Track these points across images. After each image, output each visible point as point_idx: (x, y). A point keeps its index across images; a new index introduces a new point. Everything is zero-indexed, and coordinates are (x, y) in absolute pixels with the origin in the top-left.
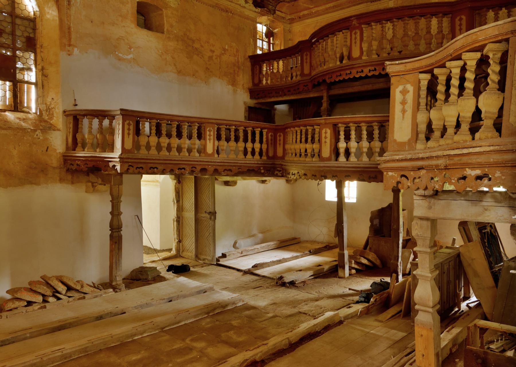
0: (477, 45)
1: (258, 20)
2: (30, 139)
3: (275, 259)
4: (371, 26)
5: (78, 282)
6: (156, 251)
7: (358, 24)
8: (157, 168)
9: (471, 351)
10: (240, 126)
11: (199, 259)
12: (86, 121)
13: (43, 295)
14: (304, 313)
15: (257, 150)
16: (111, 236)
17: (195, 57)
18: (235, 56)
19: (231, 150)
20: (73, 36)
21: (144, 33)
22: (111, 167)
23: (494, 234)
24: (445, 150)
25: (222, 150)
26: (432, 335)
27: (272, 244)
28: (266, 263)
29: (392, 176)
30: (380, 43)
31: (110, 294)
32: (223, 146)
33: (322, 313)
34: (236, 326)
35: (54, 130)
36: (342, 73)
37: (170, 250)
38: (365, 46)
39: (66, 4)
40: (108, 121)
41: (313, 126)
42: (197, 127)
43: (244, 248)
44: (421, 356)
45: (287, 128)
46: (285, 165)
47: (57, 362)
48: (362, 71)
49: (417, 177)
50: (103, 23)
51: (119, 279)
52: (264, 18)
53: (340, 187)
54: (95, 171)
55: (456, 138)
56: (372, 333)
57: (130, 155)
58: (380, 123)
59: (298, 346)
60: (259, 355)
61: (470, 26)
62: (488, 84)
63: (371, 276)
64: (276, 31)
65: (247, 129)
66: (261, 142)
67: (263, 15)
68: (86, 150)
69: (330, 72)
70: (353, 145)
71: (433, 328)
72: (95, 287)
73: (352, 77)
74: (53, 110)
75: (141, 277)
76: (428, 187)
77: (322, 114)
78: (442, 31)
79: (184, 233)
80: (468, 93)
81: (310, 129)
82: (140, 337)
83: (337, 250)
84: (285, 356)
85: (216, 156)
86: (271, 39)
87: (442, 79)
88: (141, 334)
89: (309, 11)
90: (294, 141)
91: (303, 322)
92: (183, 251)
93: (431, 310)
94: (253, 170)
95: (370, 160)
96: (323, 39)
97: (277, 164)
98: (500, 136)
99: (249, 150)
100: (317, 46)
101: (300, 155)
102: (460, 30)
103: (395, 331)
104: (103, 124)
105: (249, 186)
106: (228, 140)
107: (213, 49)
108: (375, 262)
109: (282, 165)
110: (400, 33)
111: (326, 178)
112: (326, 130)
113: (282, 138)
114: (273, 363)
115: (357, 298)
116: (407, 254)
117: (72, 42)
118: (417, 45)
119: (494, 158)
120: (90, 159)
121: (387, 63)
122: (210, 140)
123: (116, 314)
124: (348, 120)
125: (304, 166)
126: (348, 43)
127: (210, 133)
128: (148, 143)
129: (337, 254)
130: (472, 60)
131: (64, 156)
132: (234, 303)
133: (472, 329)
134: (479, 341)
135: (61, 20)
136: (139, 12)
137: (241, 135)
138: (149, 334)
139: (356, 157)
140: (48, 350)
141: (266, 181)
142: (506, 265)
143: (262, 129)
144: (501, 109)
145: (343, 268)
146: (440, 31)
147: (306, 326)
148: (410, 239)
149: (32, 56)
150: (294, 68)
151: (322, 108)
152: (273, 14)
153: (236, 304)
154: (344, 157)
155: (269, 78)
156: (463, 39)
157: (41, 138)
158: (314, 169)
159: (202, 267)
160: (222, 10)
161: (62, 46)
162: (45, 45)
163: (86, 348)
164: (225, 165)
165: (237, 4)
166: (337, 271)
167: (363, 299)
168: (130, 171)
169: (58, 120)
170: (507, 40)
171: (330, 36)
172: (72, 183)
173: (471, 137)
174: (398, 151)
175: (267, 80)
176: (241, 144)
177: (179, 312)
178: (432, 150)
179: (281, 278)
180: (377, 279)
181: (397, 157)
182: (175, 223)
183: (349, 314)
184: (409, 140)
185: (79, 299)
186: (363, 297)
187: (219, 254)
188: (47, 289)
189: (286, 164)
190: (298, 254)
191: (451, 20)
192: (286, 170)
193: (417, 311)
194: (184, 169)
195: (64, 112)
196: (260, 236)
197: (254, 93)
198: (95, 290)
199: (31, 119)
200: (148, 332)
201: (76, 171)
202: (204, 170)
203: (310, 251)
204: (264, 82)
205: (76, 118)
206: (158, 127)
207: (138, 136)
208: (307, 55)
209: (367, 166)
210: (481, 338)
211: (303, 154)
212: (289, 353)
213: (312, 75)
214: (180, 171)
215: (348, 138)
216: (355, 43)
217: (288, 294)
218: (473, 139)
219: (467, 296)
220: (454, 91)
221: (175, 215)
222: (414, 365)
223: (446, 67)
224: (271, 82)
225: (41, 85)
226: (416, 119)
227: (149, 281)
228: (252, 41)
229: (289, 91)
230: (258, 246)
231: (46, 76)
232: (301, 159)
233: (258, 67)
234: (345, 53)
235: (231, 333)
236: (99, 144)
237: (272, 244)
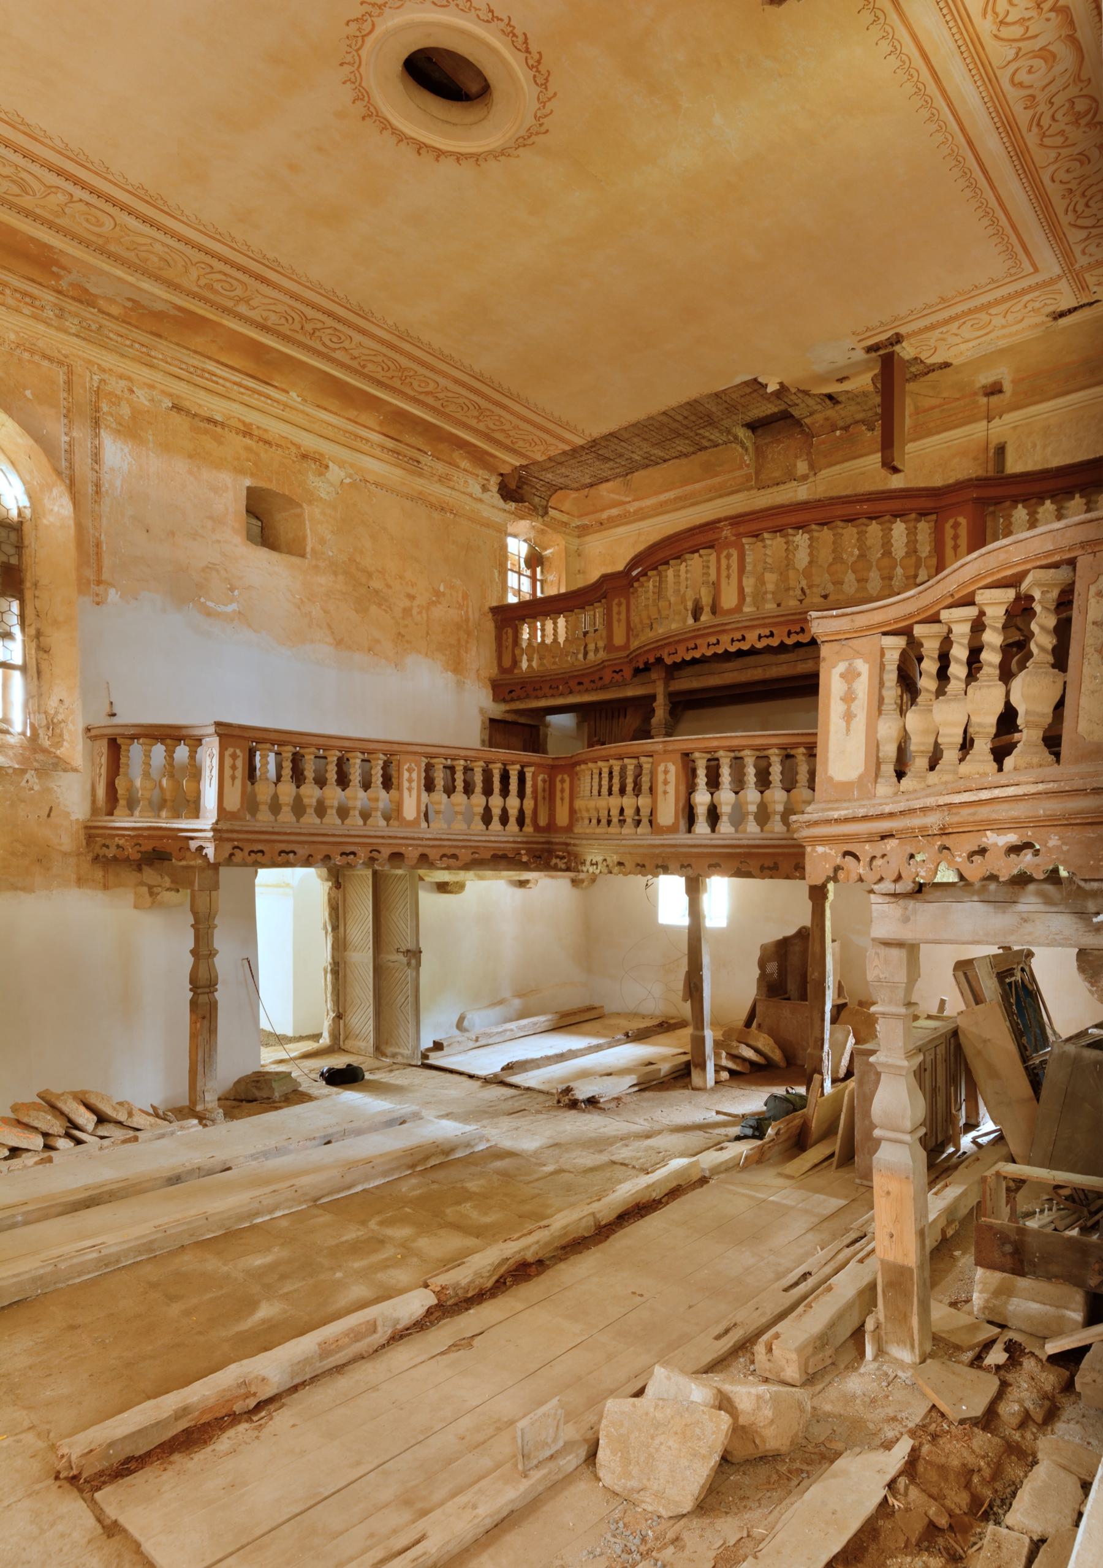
0: (1009, 572)
1: (510, 529)
2: (12, 789)
3: (551, 1052)
4: (763, 540)
5: (121, 1104)
6: (282, 1040)
7: (735, 535)
8: (295, 853)
9: (990, 1227)
10: (476, 759)
11: (384, 1055)
12: (135, 751)
13: (45, 1135)
14: (622, 1164)
15: (513, 813)
16: (194, 1004)
17: (373, 609)
18: (460, 607)
19: (457, 813)
20: (107, 561)
21: (263, 555)
22: (193, 850)
23: (1029, 986)
24: (941, 794)
25: (437, 812)
26: (909, 1190)
27: (542, 1020)
28: (533, 1061)
29: (825, 854)
30: (783, 575)
31: (192, 1130)
32: (440, 803)
33: (663, 1162)
34: (475, 1193)
35: (65, 770)
36: (698, 642)
37: (316, 1037)
38: (749, 584)
39: (90, 490)
40: (187, 748)
41: (637, 758)
42: (381, 762)
43: (482, 1030)
44: (887, 1237)
45: (579, 763)
46: (574, 845)
47: (89, 1273)
48: (744, 638)
49: (879, 855)
50: (173, 534)
51: (211, 1099)
52: (523, 526)
53: (694, 889)
54: (150, 861)
55: (964, 768)
56: (773, 1202)
57: (237, 825)
58: (785, 749)
59: (614, 1232)
60: (532, 1249)
61: (978, 541)
62: (1030, 655)
63: (761, 1085)
64: (547, 552)
65: (491, 766)
66: (521, 794)
67: (522, 518)
68: (137, 813)
69: (671, 642)
70: (726, 797)
71: (911, 1176)
72: (157, 1116)
73: (720, 652)
74: (62, 725)
75: (255, 1094)
76: (903, 875)
77: (653, 732)
78: (916, 552)
79: (348, 998)
80: (988, 675)
81: (631, 764)
82: (267, 1218)
83: (688, 1031)
84: (587, 1253)
85: (424, 825)
86: (539, 570)
87: (930, 648)
88: (271, 1212)
89: (621, 508)
90: (595, 792)
91: (620, 1182)
92: (346, 1038)
93: (907, 1138)
94: (504, 857)
95: (762, 831)
96: (656, 568)
97: (557, 844)
98: (1058, 761)
99: (496, 812)
100: (642, 586)
101: (609, 822)
102: (956, 547)
103: (822, 1197)
104: (175, 755)
105: (489, 893)
106: (450, 790)
107: (412, 591)
108: (770, 1054)
109: (567, 844)
110: (825, 555)
111: (666, 870)
112: (666, 767)
113: (567, 786)
114: (562, 1266)
115: (736, 1131)
116: (839, 1036)
117: (106, 575)
118: (862, 581)
119: (1044, 808)
120: (146, 833)
121: (814, 614)
122: (410, 789)
123: (211, 1172)
124: (715, 743)
125: (618, 845)
126: (713, 577)
127: (410, 777)
128: (275, 797)
129: (688, 1040)
130: (995, 604)
131: (86, 827)
132: (468, 1145)
133: (991, 1181)
134: (1006, 1210)
135: (80, 527)
136: (251, 511)
137: (478, 778)
138: (287, 1212)
139: (732, 825)
140: (69, 1248)
141: (528, 881)
142: (1056, 1051)
143: (522, 767)
144: (1060, 705)
145: (703, 1067)
146: (912, 550)
147: (630, 1189)
148: (845, 1005)
149: (15, 606)
150: (591, 634)
151: (654, 721)
152: (542, 517)
153: (472, 1147)
154: (706, 825)
155: (535, 656)
156: (969, 567)
157: (37, 788)
158: (641, 850)
159: (391, 1071)
160: (432, 505)
161: (83, 585)
162: (44, 581)
163: (151, 1242)
164: (444, 846)
165: (464, 493)
166: (689, 1074)
167: (749, 1132)
168: (236, 859)
169: (74, 748)
170: (1072, 563)
171: (671, 562)
172: (106, 887)
173: (995, 766)
174: (837, 801)
175: (530, 660)
176: (478, 800)
177: (351, 1165)
178: (912, 796)
179: (568, 1090)
180: (780, 1091)
181: (835, 815)
182: (329, 976)
183: (722, 1163)
184: (861, 777)
185: (124, 1142)
186: (751, 1127)
187: (426, 1043)
188: (54, 1121)
189: (577, 842)
190: (601, 1041)
191: (936, 527)
192: (576, 856)
193: (878, 1142)
194: (354, 854)
195: (88, 730)
196: (517, 1003)
197: (501, 689)
198: (159, 1121)
199: (12, 747)
200: (284, 1209)
201: (115, 859)
202: (397, 857)
203: (627, 1035)
204: (524, 665)
205: (115, 746)
206: (297, 760)
207: (253, 784)
208: (619, 604)
209: (757, 842)
210: (1011, 1200)
211: (615, 820)
212: (596, 1245)
213: (632, 648)
214: (345, 859)
215: (714, 783)
216: (728, 577)
217: (586, 1125)
218: (1000, 769)
219: (973, 1122)
220: (959, 670)
221: (329, 959)
222: (866, 1262)
223: (939, 622)
224: (541, 665)
225: (35, 670)
226: (876, 732)
227: (274, 1102)
228: (496, 574)
229: (580, 683)
230: (513, 1025)
231: (46, 652)
232: (611, 830)
233: (510, 631)
234: (706, 601)
235: (467, 1208)
236: (165, 801)
237: (542, 1020)
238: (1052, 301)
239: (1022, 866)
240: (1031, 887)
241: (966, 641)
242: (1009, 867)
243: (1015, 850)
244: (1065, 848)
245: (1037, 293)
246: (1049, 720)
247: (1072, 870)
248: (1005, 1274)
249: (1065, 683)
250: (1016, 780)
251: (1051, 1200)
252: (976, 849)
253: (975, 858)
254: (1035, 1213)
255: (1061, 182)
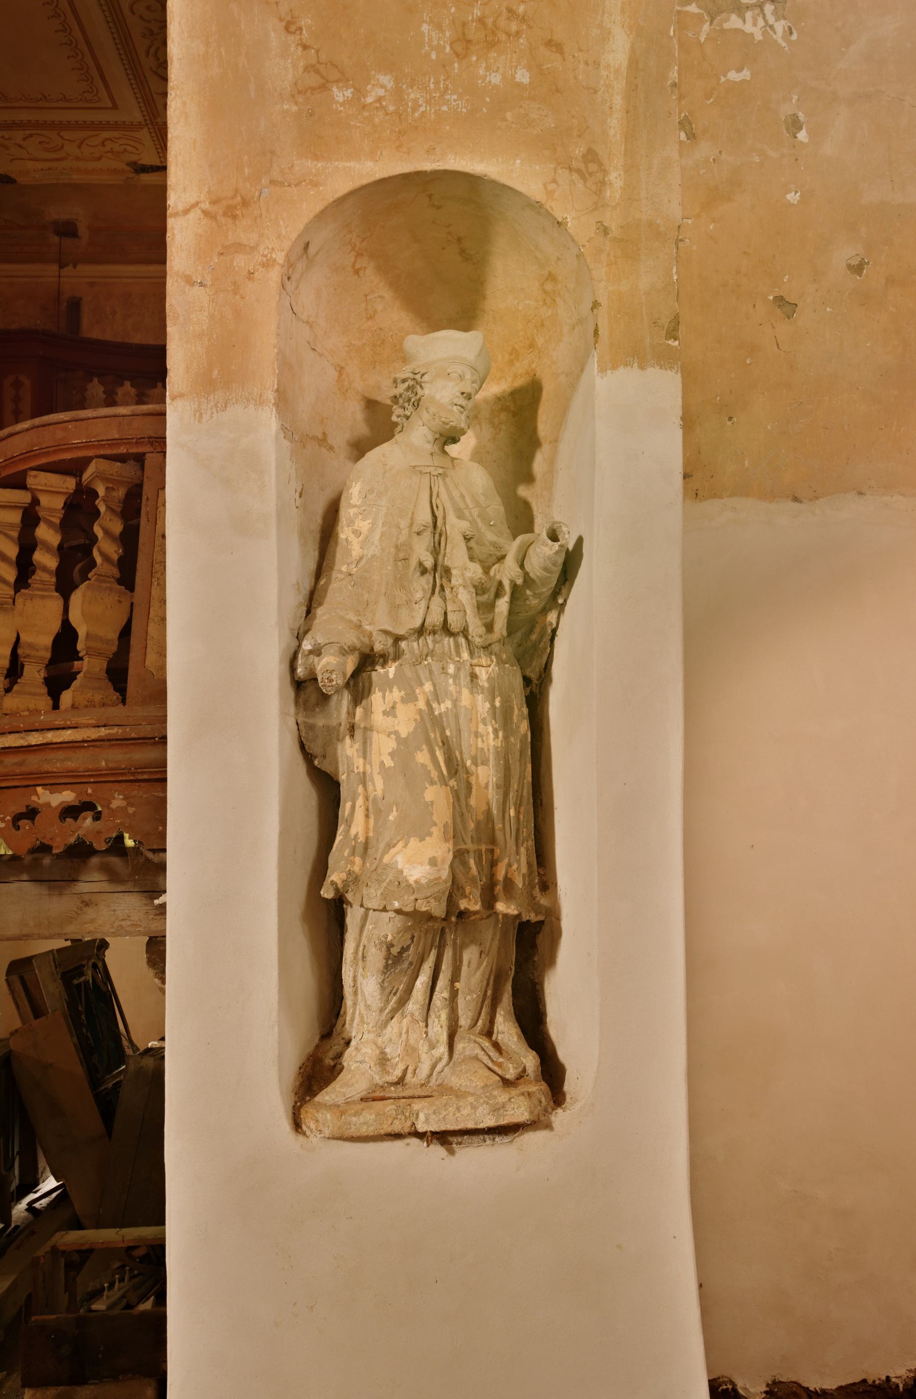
0: (67, 456)
62: (93, 564)
80: (42, 582)
144: (126, 633)
218: (56, 706)
238: (134, 150)
239: (80, 833)
240: (95, 861)
241: (15, 534)
242: (62, 836)
243: (70, 812)
244: (131, 810)
245: (115, 134)
246: (114, 648)
247: (138, 838)
248: (62, 1388)
249: (132, 604)
250: (74, 721)
251: (123, 1266)
252: (24, 810)
253: (22, 823)
254: (103, 1289)
255: (141, 17)
